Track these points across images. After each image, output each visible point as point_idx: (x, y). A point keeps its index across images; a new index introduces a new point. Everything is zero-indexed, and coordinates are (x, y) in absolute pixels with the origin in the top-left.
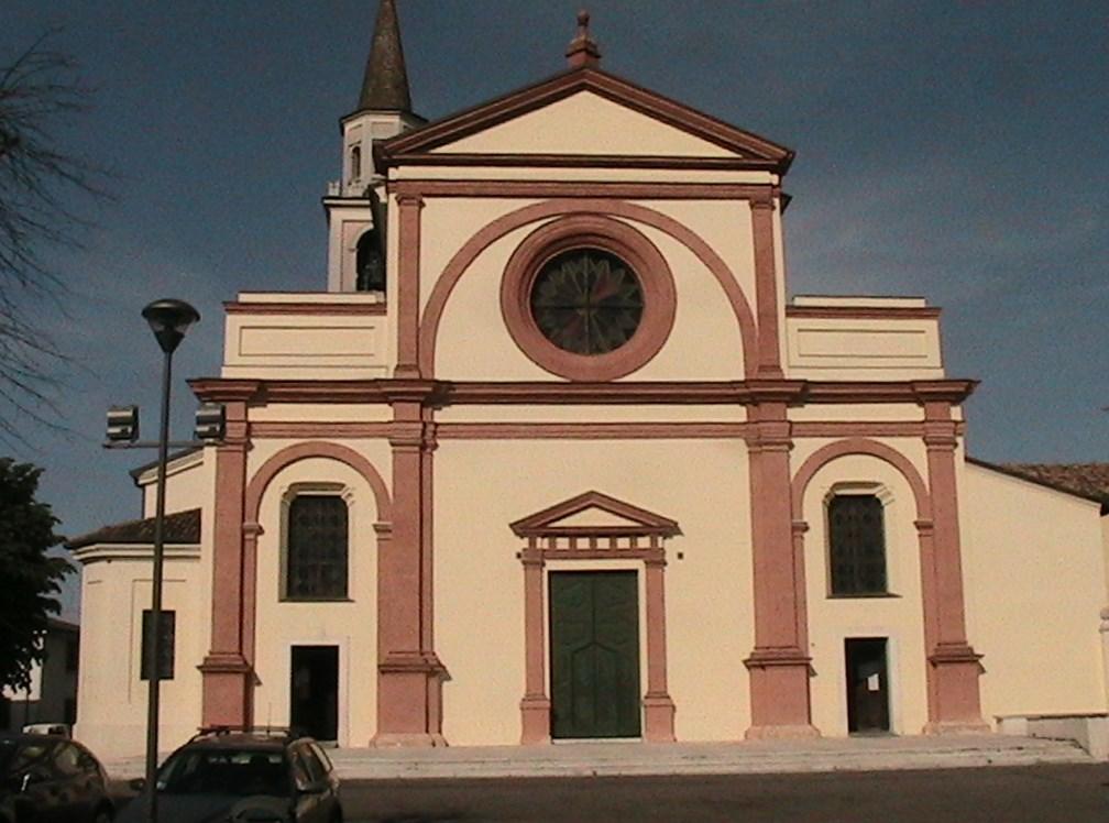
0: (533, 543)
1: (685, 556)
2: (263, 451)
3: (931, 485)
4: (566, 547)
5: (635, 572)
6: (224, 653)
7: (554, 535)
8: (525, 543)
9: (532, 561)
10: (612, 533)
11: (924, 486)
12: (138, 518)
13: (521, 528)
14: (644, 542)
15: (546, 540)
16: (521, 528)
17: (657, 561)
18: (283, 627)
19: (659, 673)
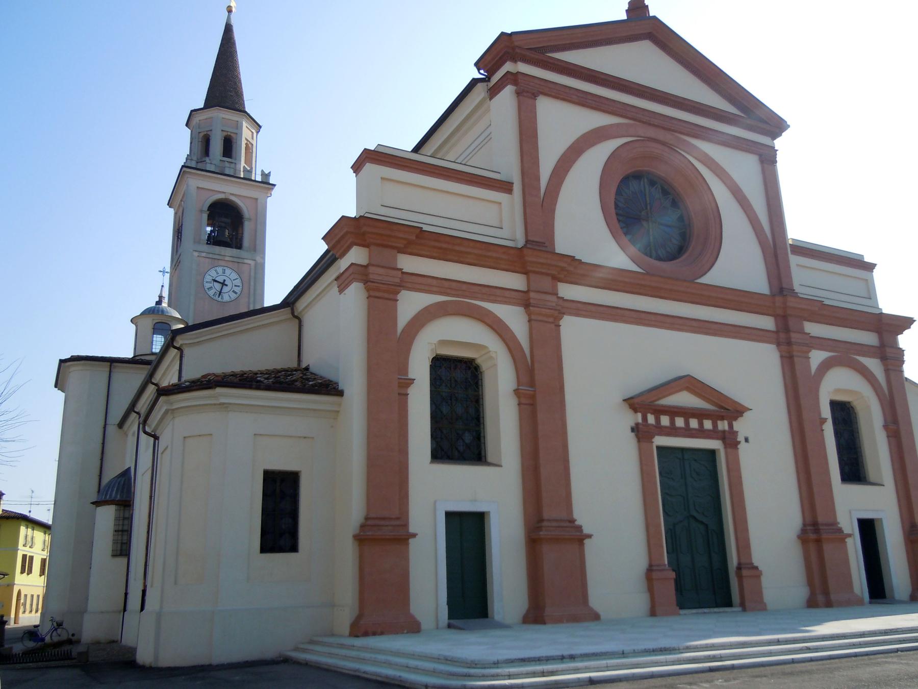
0: (645, 419)
1: (750, 440)
2: (410, 304)
3: (630, 119)
4: (720, 423)
5: (712, 453)
6: (384, 519)
7: (659, 411)
8: (639, 417)
9: (641, 433)
10: (700, 415)
11: (618, 125)
12: (294, 365)
13: (633, 403)
14: (723, 425)
15: (726, 422)
16: (633, 403)
17: (731, 440)
18: (437, 490)
19: (744, 545)
